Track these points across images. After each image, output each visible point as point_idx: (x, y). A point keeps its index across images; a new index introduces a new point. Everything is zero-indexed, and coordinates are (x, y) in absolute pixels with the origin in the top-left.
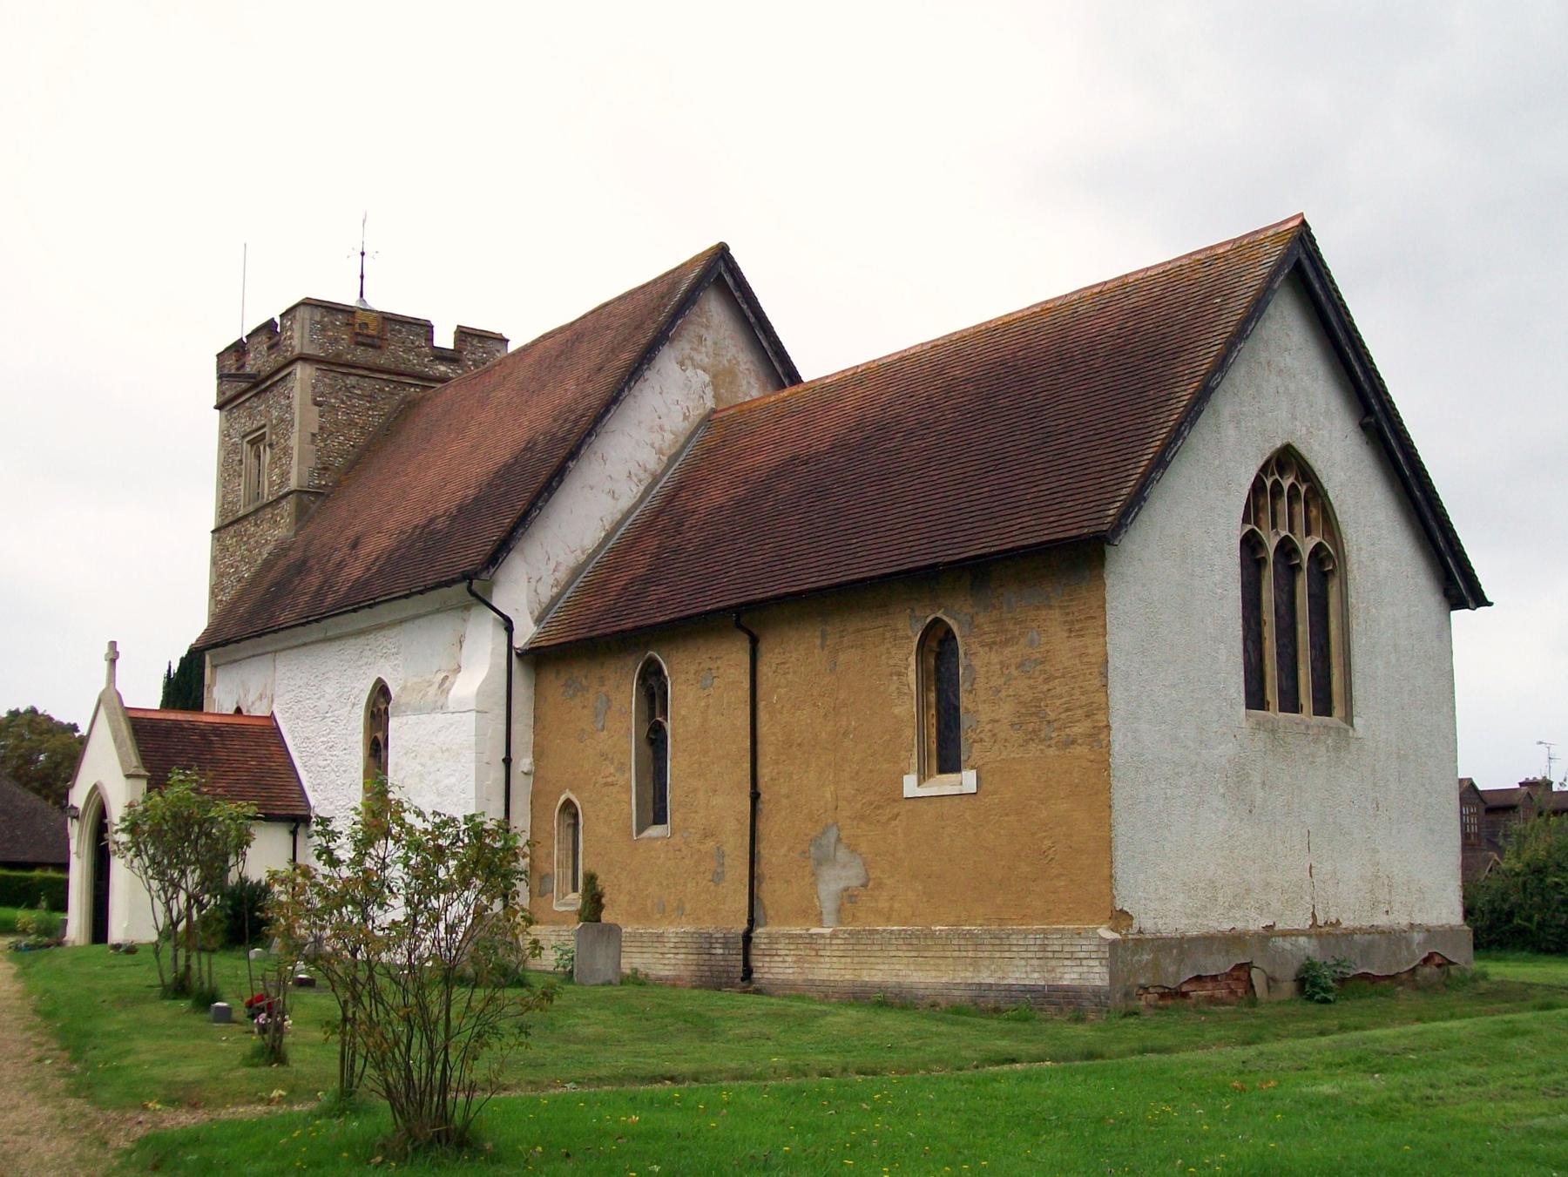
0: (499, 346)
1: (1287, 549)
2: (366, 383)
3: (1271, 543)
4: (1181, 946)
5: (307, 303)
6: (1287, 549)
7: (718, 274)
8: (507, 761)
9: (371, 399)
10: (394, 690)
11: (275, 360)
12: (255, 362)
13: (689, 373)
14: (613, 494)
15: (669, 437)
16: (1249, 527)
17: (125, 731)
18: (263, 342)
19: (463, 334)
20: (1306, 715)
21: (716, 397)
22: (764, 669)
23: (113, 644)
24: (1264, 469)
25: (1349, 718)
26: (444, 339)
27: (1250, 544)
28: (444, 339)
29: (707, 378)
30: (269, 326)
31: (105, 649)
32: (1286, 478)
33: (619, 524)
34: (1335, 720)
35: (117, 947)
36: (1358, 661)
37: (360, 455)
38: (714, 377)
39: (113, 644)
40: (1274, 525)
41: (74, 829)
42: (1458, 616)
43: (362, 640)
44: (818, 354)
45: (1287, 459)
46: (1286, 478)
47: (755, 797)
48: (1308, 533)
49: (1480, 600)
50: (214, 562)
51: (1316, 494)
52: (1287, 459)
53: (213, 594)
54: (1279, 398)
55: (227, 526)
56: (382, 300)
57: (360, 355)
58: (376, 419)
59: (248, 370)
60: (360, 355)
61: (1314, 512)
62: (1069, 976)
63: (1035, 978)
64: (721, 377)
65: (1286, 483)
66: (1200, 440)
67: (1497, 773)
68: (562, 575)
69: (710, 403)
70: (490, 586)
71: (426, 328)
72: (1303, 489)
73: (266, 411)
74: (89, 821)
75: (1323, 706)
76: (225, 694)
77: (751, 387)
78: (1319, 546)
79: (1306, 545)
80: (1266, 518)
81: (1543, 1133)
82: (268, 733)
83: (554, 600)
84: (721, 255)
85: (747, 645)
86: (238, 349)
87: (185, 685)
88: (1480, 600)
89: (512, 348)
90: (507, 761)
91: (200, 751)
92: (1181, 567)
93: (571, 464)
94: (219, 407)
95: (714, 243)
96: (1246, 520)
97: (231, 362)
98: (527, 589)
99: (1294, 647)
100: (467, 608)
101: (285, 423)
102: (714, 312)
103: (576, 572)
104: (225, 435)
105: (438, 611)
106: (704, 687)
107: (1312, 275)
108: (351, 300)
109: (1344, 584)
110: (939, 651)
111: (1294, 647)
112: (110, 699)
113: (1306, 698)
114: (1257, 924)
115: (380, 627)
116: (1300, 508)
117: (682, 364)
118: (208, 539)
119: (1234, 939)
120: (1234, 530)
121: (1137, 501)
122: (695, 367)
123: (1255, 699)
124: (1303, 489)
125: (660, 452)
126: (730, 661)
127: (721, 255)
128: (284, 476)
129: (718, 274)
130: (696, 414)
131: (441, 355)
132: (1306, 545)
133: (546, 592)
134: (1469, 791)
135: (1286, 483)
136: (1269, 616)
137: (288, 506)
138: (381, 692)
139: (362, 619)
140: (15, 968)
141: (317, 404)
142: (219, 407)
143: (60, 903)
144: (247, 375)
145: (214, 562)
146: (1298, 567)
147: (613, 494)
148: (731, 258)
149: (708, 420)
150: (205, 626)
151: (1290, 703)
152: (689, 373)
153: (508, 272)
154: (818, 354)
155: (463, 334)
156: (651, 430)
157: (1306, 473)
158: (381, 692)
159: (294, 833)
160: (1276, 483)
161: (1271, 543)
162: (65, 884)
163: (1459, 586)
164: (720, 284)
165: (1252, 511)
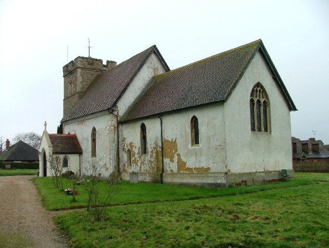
1: (259, 101)
3: (256, 101)
4: (240, 175)
5: (79, 57)
6: (259, 101)
7: (154, 50)
11: (74, 68)
12: (70, 68)
15: (146, 82)
18: (71, 65)
19: (108, 62)
23: (45, 122)
24: (254, 87)
25: (270, 132)
26: (105, 63)
27: (252, 101)
28: (105, 63)
30: (72, 62)
32: (258, 89)
36: (272, 122)
37: (89, 83)
39: (45, 122)
41: (40, 156)
42: (292, 113)
44: (172, 67)
45: (258, 85)
46: (258, 89)
49: (295, 109)
50: (64, 106)
51: (264, 91)
52: (258, 85)
54: (256, 72)
56: (93, 56)
58: (92, 78)
59: (69, 70)
60: (89, 66)
62: (219, 181)
63: (213, 182)
64: (155, 70)
65: (258, 89)
66: (241, 82)
67: (304, 137)
72: (262, 90)
74: (42, 155)
75: (266, 130)
76: (67, 130)
77: (161, 71)
79: (262, 101)
84: (155, 47)
86: (67, 66)
87: (60, 130)
88: (295, 109)
89: (117, 64)
91: (66, 144)
92: (240, 101)
95: (151, 45)
96: (251, 96)
99: (260, 119)
101: (76, 80)
102: (153, 57)
109: (269, 107)
111: (260, 119)
112: (45, 132)
113: (263, 128)
114: (254, 171)
115: (270, 127)
116: (261, 94)
119: (250, 173)
120: (249, 98)
121: (230, 94)
123: (253, 129)
124: (262, 90)
126: (158, 121)
128: (76, 89)
129: (154, 50)
130: (151, 76)
132: (262, 101)
134: (295, 142)
135: (258, 89)
136: (255, 114)
137: (77, 95)
138: (94, 130)
143: (38, 167)
144: (70, 70)
149: (153, 78)
151: (260, 130)
153: (115, 50)
155: (108, 62)
157: (262, 87)
158: (94, 130)
159: (80, 156)
161: (256, 101)
162: (38, 164)
163: (291, 107)
164: (154, 52)
165: (252, 95)
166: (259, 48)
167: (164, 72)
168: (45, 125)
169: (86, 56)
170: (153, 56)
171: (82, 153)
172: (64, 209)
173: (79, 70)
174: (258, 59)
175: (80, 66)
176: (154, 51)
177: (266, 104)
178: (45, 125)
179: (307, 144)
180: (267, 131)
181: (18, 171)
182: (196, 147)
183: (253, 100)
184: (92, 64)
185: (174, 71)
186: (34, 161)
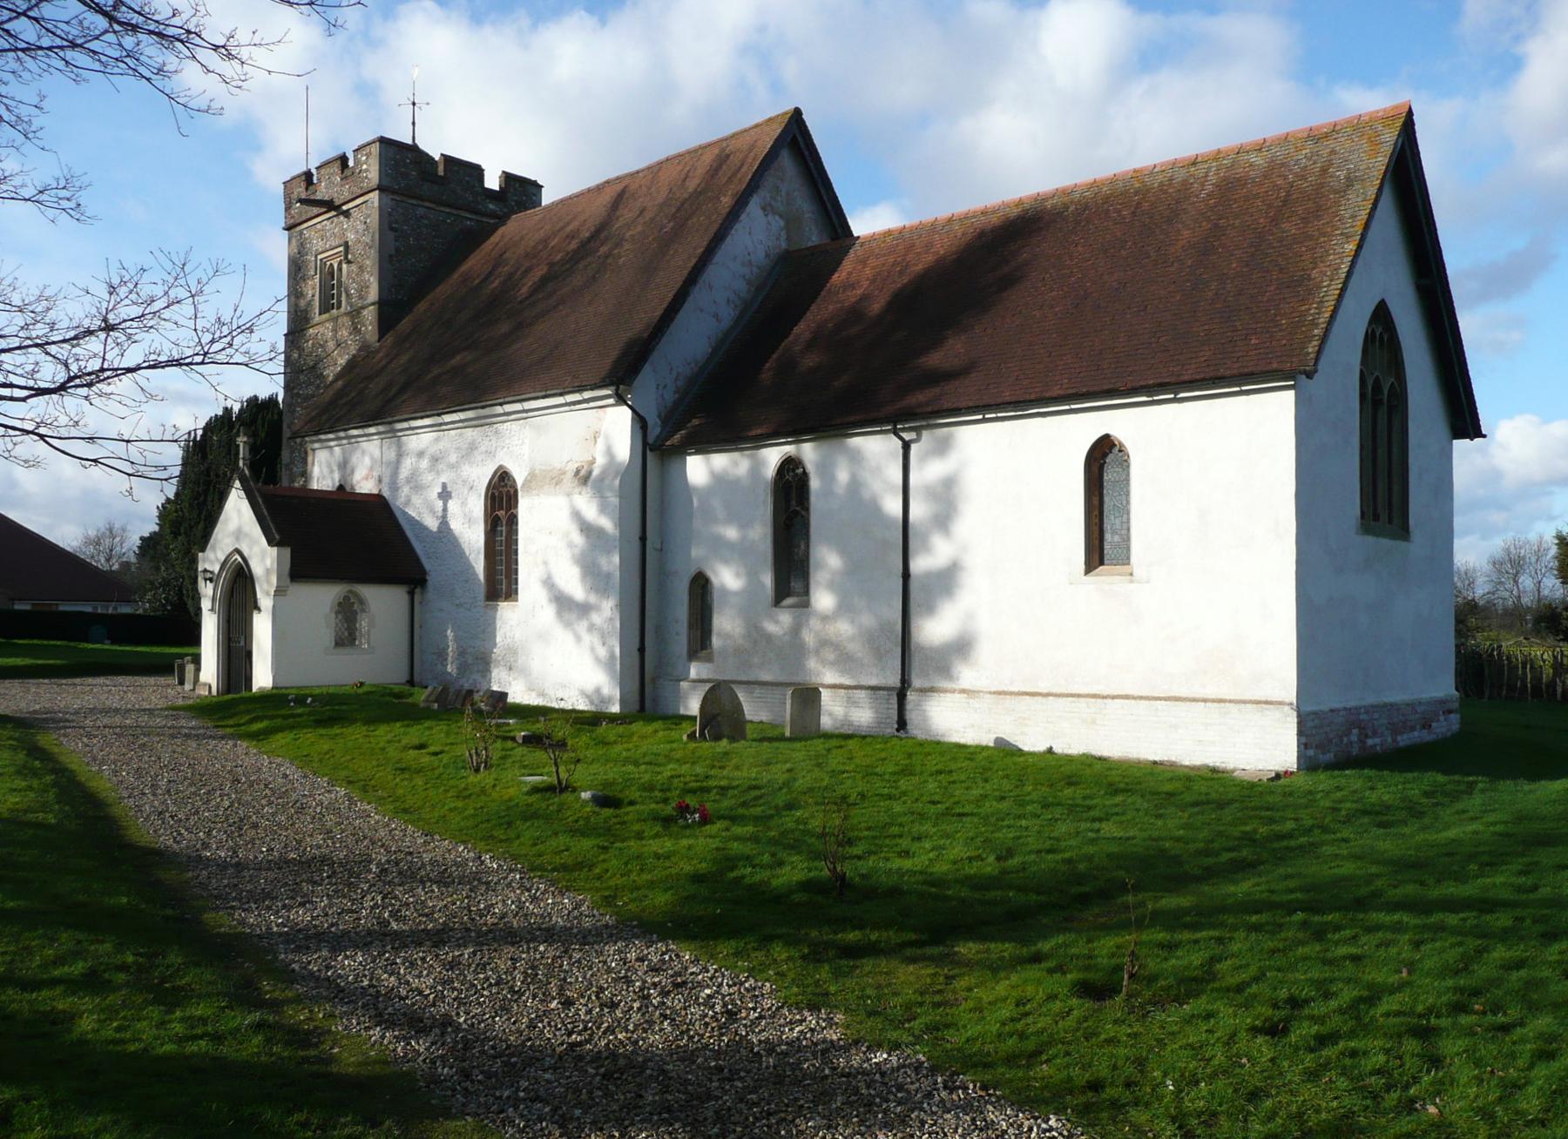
8: (643, 539)
10: (519, 477)
19: (508, 178)
26: (492, 182)
28: (492, 182)
29: (782, 223)
35: (694, 681)
38: (787, 222)
42: (1460, 445)
64: (792, 223)
69: (784, 245)
71: (476, 171)
83: (676, 404)
97: (300, 191)
108: (410, 142)
122: (774, 213)
140: (510, 700)
141: (392, 229)
148: (803, 122)
155: (508, 178)
159: (411, 594)
163: (1465, 422)
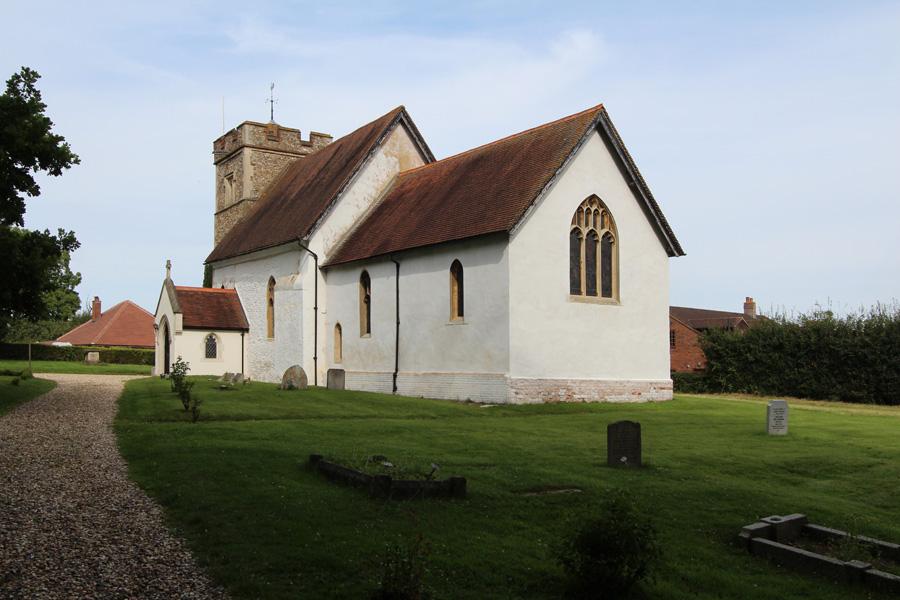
0: (328, 140)
1: (592, 234)
2: (273, 156)
3: (585, 231)
6: (592, 234)
7: (400, 117)
9: (275, 162)
11: (234, 147)
12: (228, 147)
13: (389, 158)
14: (358, 206)
16: (574, 226)
17: (174, 296)
19: (313, 135)
20: (584, 296)
21: (401, 167)
22: (400, 278)
23: (169, 262)
27: (575, 233)
28: (305, 137)
31: (166, 264)
32: (593, 207)
33: (361, 217)
34: (613, 299)
39: (169, 262)
40: (587, 225)
43: (265, 261)
46: (593, 207)
47: (398, 323)
48: (603, 227)
49: (681, 253)
53: (216, 240)
54: (591, 171)
55: (221, 212)
57: (270, 144)
60: (270, 144)
61: (606, 220)
64: (402, 159)
65: (593, 210)
68: (337, 238)
69: (398, 170)
70: (308, 242)
72: (601, 211)
73: (233, 167)
77: (416, 162)
78: (607, 233)
79: (601, 233)
80: (583, 223)
81: (795, 484)
82: (234, 296)
84: (402, 109)
85: (395, 265)
88: (681, 253)
89: (334, 140)
90: (316, 308)
92: (543, 236)
93: (340, 195)
94: (216, 164)
97: (219, 145)
98: (325, 239)
99: (593, 266)
100: (300, 250)
101: (241, 172)
103: (343, 236)
104: (218, 175)
105: (290, 251)
106: (382, 282)
107: (606, 128)
109: (618, 247)
110: (457, 271)
111: (593, 266)
113: (583, 288)
115: (271, 256)
116: (599, 219)
117: (385, 154)
118: (212, 219)
120: (569, 228)
123: (575, 289)
124: (601, 211)
125: (378, 189)
127: (402, 109)
129: (400, 117)
131: (305, 144)
132: (601, 233)
133: (331, 244)
139: (264, 253)
142: (216, 164)
145: (216, 227)
146: (597, 241)
147: (358, 206)
149: (398, 177)
150: (213, 249)
151: (591, 292)
152: (389, 158)
154: (441, 154)
155: (313, 135)
156: (373, 181)
157: (602, 204)
159: (243, 335)
160: (588, 209)
161: (585, 231)
164: (401, 122)
166: (599, 123)
167: (424, 164)
168: (169, 267)
169: (266, 121)
170: (399, 130)
171: (247, 330)
172: (423, 417)
173: (247, 152)
174: (595, 145)
175: (248, 142)
176: (401, 120)
177: (609, 241)
178: (169, 267)
179: (186, 327)
180: (610, 295)
181: (114, 366)
182: (366, 340)
183: (580, 232)
184: (277, 139)
185: (447, 162)
186: (150, 347)
